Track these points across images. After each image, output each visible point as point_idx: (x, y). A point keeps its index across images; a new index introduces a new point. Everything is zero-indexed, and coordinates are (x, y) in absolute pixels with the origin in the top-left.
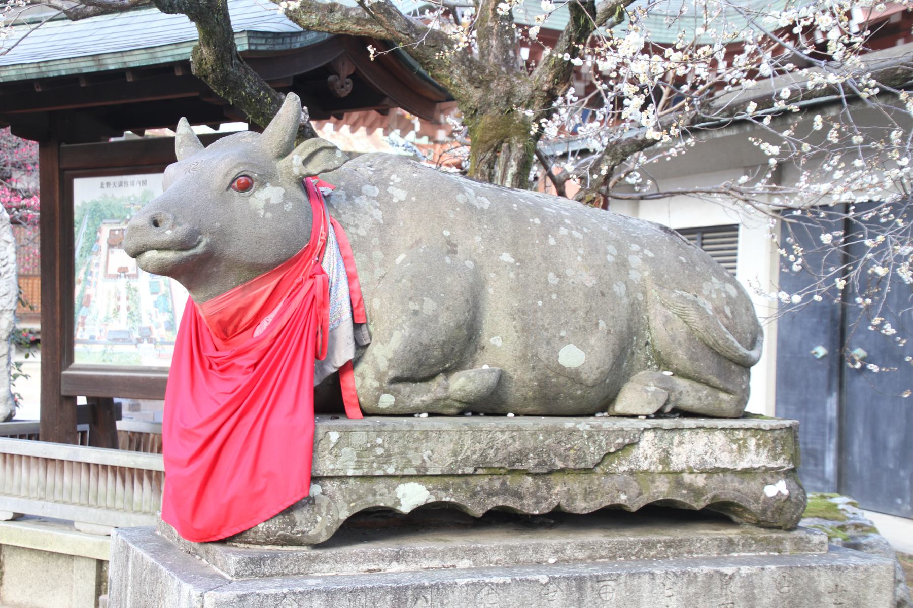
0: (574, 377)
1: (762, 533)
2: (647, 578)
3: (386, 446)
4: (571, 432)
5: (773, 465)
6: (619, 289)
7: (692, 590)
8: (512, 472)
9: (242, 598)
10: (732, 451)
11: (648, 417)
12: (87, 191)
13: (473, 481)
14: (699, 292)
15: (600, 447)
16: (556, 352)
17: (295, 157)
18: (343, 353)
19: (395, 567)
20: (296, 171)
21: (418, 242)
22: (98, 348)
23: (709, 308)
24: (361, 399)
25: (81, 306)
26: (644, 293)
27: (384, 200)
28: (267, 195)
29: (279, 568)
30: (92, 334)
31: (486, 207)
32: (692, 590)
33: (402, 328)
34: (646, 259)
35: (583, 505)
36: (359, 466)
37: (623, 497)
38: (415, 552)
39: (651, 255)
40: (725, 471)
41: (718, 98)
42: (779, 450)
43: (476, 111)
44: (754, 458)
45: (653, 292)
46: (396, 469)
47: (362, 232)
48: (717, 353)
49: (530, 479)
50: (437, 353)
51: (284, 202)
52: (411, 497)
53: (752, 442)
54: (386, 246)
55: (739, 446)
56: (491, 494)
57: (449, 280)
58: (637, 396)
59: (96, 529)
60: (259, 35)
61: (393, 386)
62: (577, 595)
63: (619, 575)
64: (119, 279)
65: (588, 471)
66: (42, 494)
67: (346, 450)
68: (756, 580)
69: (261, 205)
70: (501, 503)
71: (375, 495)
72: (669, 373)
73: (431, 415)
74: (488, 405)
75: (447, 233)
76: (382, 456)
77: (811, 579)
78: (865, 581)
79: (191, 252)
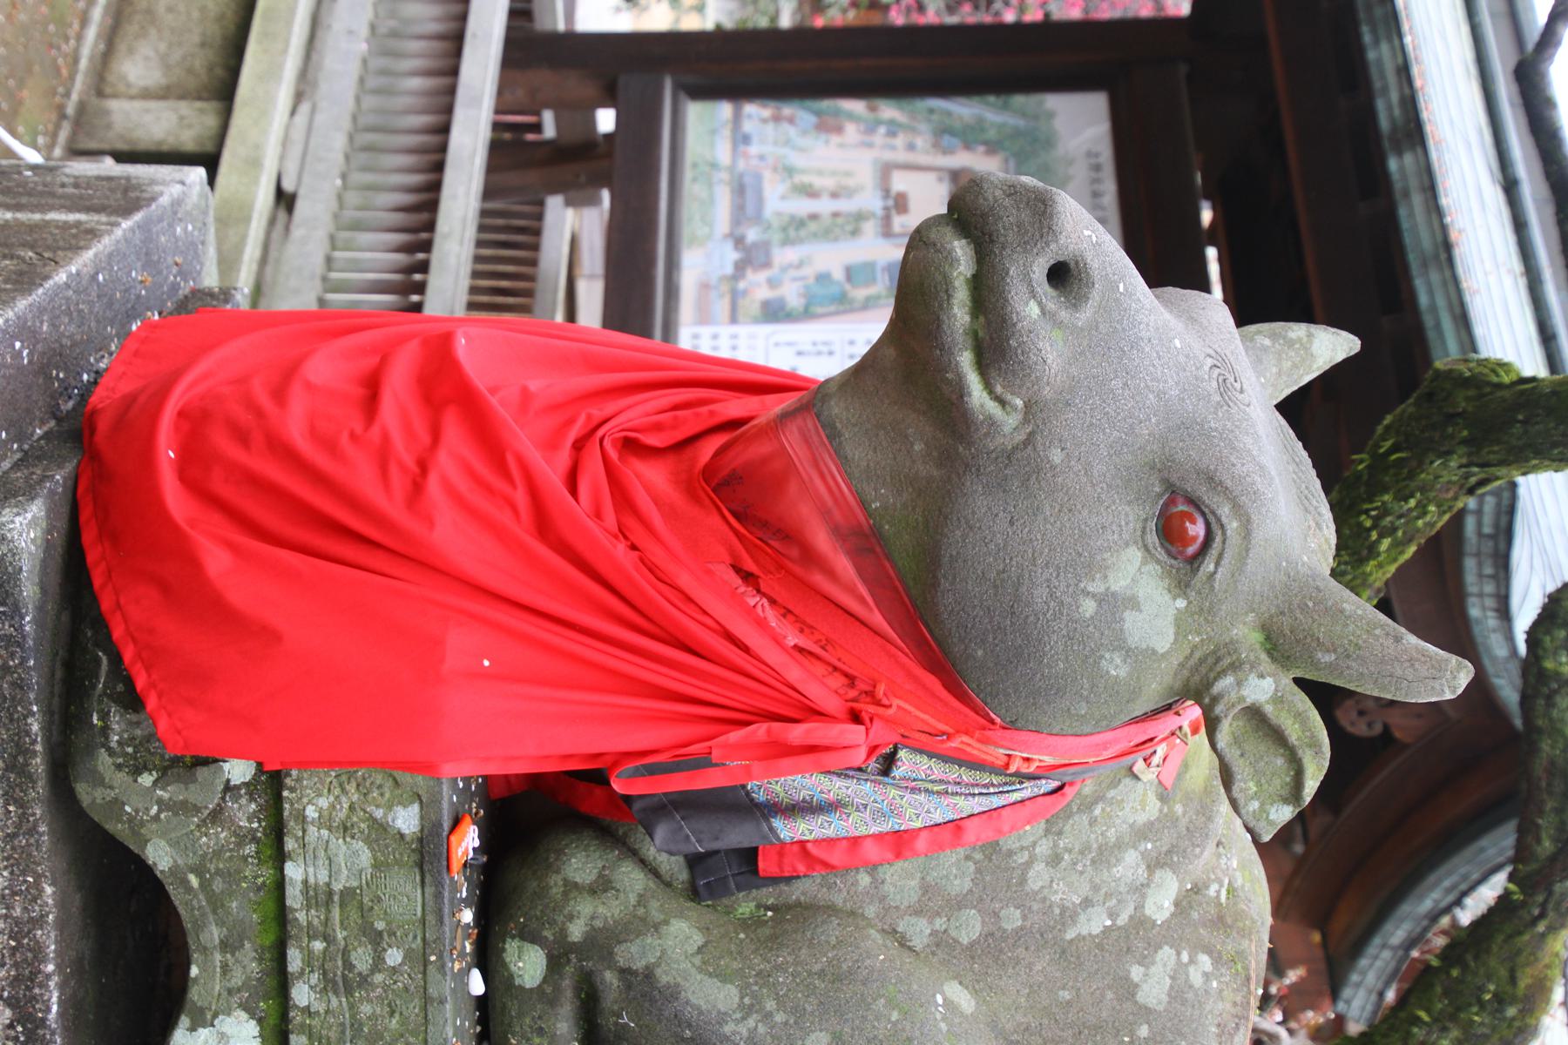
3: (378, 978)
12: (1080, 123)
22: (723, 152)
25: (818, 113)
30: (755, 139)
33: (747, 1011)
36: (319, 897)
41: (834, 173)
46: (307, 1011)
59: (295, 151)
60: (1504, 520)
64: (879, 194)
66: (382, 30)
69: (1119, 582)
76: (348, 965)
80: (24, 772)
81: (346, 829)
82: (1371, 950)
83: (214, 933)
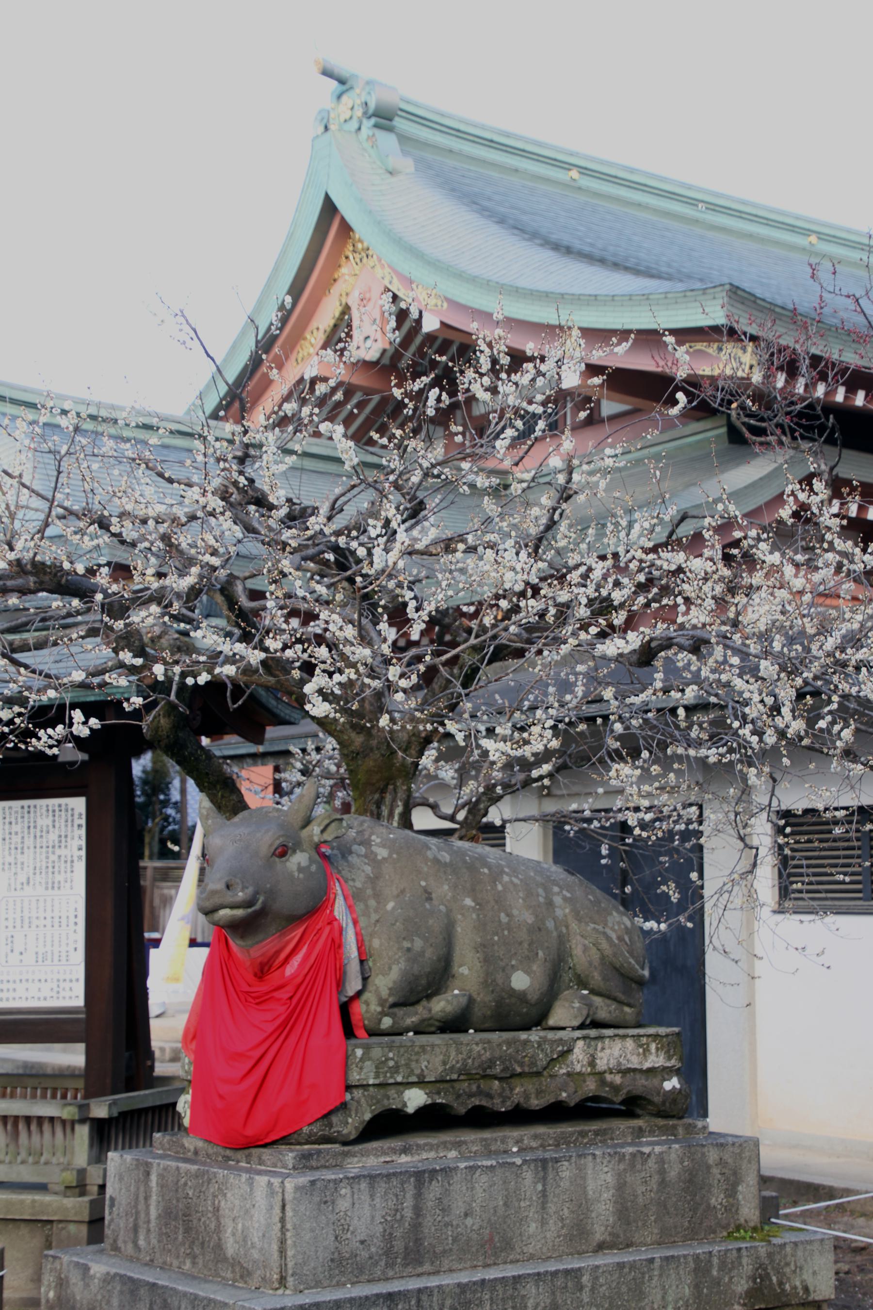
0: (521, 997)
1: (661, 1122)
2: (590, 1158)
4: (526, 1042)
5: (668, 1064)
6: (550, 924)
7: (622, 1167)
8: (485, 1077)
9: (313, 1183)
10: (639, 1054)
11: (574, 1029)
13: (457, 1085)
14: (606, 924)
15: (547, 1055)
16: (508, 978)
17: (315, 828)
18: (353, 985)
19: (404, 1159)
20: (316, 839)
21: (403, 892)
23: (614, 936)
24: (366, 1022)
26: (567, 927)
27: (371, 857)
28: (299, 859)
29: (322, 1162)
31: (448, 860)
32: (622, 1167)
34: (565, 899)
35: (536, 1102)
36: (377, 1076)
37: (564, 1095)
38: (418, 1146)
39: (568, 895)
40: (634, 1070)
42: (672, 1052)
43: (358, 754)
44: (655, 1059)
45: (574, 926)
47: (358, 884)
48: (622, 975)
49: (497, 1082)
50: (424, 982)
51: (310, 865)
52: (415, 1099)
53: (653, 1046)
54: (377, 896)
55: (644, 1050)
56: (471, 1095)
57: (431, 922)
58: (565, 1013)
61: (391, 1010)
62: (542, 1174)
63: (571, 1157)
65: (538, 1074)
67: (368, 1063)
68: (666, 1158)
69: (295, 868)
70: (477, 1103)
71: (388, 1099)
72: (585, 992)
73: (416, 1033)
74: (454, 1025)
75: (423, 883)
77: (703, 1154)
78: (740, 1154)
79: (253, 909)
80: (349, 1152)
81: (361, 1068)
82: (278, 711)
83: (386, 1102)
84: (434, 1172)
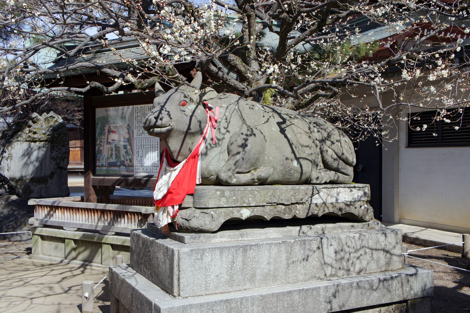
52: (245, 214)
84: (251, 246)
